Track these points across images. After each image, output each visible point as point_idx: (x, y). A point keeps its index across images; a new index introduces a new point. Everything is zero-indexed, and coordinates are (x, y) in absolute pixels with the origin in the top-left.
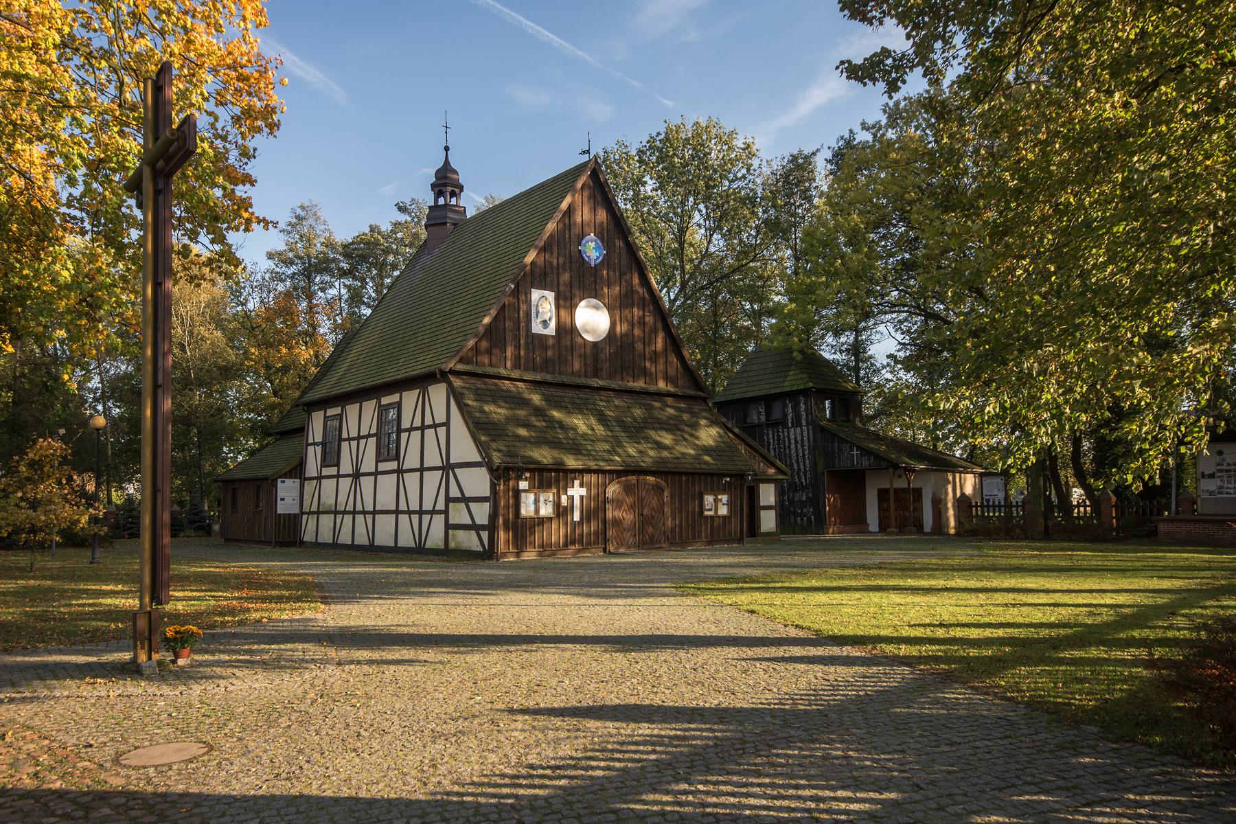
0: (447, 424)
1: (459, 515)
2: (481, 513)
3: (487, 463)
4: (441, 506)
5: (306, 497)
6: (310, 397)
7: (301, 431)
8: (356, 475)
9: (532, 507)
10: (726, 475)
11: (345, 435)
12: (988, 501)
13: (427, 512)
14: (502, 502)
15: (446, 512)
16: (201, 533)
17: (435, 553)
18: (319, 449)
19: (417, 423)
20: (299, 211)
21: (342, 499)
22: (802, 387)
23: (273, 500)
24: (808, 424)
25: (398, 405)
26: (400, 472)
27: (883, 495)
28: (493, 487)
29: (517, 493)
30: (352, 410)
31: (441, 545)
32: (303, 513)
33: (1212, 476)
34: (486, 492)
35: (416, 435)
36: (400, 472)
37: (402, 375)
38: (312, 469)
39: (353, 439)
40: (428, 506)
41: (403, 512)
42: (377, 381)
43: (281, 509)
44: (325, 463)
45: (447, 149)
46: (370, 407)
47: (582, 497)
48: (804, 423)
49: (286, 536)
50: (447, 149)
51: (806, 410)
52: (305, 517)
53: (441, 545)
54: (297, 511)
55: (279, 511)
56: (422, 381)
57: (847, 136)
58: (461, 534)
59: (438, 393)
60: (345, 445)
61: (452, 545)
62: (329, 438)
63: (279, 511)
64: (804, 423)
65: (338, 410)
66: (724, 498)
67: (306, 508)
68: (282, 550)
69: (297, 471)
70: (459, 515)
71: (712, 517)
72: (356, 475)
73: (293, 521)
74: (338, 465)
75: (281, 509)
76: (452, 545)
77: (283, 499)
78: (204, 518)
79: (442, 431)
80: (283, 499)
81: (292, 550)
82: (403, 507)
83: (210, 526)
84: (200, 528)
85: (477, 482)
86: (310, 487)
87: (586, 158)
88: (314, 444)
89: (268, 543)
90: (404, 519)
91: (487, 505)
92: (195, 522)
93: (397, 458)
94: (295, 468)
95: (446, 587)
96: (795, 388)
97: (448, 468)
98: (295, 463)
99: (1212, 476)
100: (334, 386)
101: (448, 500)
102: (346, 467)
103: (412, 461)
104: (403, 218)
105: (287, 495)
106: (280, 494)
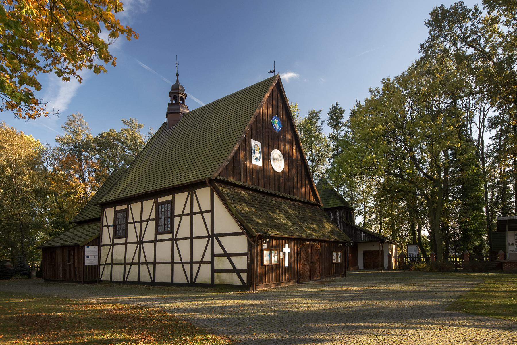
0: (212, 211)
1: (222, 264)
2: (241, 263)
3: (246, 231)
4: (208, 258)
5: (102, 255)
6: (104, 200)
7: (98, 220)
8: (140, 242)
9: (268, 258)
10: (341, 243)
11: (130, 220)
12: (410, 255)
13: (128, 264)
14: (254, 255)
15: (212, 263)
16: (26, 276)
17: (204, 286)
18: (111, 229)
19: (188, 210)
20: (72, 118)
21: (130, 256)
22: (338, 206)
23: (82, 257)
24: (340, 222)
25: (172, 203)
26: (126, 243)
27: (365, 253)
28: (250, 246)
29: (262, 250)
30: (136, 207)
31: (209, 281)
32: (100, 265)
33: (513, 244)
34: (245, 250)
35: (186, 220)
36: (174, 240)
37: (177, 182)
38: (106, 239)
39: (137, 222)
40: (197, 258)
41: (143, 264)
42: (157, 188)
43: (87, 262)
44: (115, 236)
45: (177, 75)
46: (149, 205)
47: (289, 253)
48: (338, 222)
49: (91, 278)
50: (177, 75)
51: (340, 216)
52: (102, 267)
53: (209, 281)
54: (96, 264)
55: (86, 263)
56: (191, 187)
57: (335, 104)
58: (224, 275)
59: (204, 195)
60: (131, 227)
61: (217, 281)
62: (118, 222)
63: (86, 263)
64: (338, 222)
65: (125, 207)
66: (339, 254)
67: (103, 261)
68: (87, 286)
69: (97, 241)
70: (222, 264)
71: (335, 263)
72: (140, 242)
73: (95, 269)
74: (125, 236)
75: (87, 262)
76: (217, 281)
77: (88, 257)
78: (27, 269)
79: (207, 216)
80: (88, 257)
81: (92, 286)
82: (177, 259)
83: (30, 273)
84: (24, 274)
85: (239, 244)
86: (104, 251)
87: (272, 75)
88: (108, 226)
89: (79, 282)
90: (143, 268)
91: (245, 259)
92: (21, 271)
93: (172, 231)
94: (95, 239)
95: (332, 321)
96: (335, 206)
97: (213, 237)
98: (96, 236)
99: (513, 244)
100: (122, 193)
101: (213, 255)
102: (132, 237)
103: (184, 231)
104: (126, 127)
105: (90, 255)
106: (86, 254)
